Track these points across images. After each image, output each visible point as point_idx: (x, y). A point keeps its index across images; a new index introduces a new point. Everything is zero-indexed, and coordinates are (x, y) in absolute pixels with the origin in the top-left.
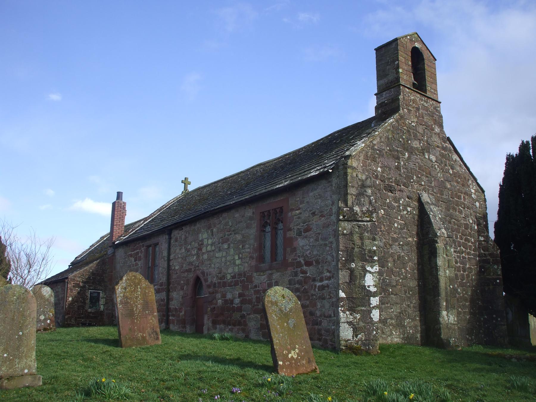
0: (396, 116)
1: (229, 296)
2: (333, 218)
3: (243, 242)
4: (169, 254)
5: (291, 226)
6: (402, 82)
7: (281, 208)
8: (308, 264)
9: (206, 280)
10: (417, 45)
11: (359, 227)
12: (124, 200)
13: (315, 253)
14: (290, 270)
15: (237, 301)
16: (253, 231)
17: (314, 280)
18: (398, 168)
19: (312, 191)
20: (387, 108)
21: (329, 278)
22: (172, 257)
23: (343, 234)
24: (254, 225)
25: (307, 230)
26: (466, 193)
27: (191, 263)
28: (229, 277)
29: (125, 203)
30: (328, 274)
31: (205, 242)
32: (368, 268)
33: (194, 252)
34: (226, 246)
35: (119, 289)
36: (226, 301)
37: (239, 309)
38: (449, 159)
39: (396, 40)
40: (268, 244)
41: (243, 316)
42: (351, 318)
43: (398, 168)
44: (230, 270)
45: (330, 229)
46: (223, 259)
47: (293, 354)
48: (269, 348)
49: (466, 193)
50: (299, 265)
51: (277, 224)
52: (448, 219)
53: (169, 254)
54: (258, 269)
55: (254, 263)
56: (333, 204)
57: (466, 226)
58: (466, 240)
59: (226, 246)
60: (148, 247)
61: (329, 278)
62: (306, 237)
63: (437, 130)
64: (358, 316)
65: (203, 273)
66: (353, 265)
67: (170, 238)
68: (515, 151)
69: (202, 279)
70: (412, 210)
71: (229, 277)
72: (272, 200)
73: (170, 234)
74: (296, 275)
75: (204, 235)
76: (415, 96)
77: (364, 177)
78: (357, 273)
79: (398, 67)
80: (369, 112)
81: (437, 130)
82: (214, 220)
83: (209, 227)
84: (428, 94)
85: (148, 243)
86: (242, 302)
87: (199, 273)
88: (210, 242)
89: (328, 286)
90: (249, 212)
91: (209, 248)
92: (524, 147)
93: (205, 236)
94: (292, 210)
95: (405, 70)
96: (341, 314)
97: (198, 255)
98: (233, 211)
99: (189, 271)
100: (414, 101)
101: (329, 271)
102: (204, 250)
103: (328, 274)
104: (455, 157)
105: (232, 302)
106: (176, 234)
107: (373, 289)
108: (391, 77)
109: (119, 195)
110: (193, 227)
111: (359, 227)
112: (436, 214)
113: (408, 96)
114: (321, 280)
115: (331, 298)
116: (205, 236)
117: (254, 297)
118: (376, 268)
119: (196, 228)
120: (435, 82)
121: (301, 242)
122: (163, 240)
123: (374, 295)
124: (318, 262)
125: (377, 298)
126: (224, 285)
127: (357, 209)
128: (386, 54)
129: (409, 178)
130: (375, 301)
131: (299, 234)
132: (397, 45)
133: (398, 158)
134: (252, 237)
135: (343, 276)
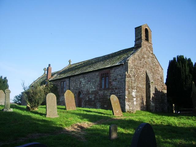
0: (141, 48)
1: (90, 97)
2: (124, 77)
3: (95, 82)
4: (69, 84)
5: (111, 78)
6: (142, 39)
7: (108, 73)
8: (116, 89)
9: (83, 93)
10: (147, 28)
11: (131, 79)
12: (51, 67)
13: (118, 86)
14: (110, 90)
15: (93, 99)
16: (98, 79)
17: (118, 93)
18: (141, 63)
19: (117, 69)
20: (138, 46)
21: (122, 93)
22: (70, 85)
23: (127, 81)
24: (99, 77)
25: (116, 79)
26: (158, 70)
27: (77, 87)
28: (90, 92)
29: (51, 68)
30: (122, 92)
31: (82, 81)
32: (133, 91)
33: (78, 84)
34: (89, 83)
35: (65, 94)
36: (89, 99)
37: (94, 101)
38: (154, 60)
39: (141, 26)
40: (103, 83)
41: (95, 103)
42: (128, 104)
43: (141, 63)
44: (91, 90)
45: (123, 80)
46: (89, 87)
47: (117, 112)
48: (112, 111)
49: (158, 70)
50: (113, 89)
51: (106, 77)
52: (153, 78)
53: (69, 84)
54: (100, 90)
55: (99, 88)
56: (124, 73)
57: (158, 79)
58: (158, 83)
59: (89, 83)
60: (61, 82)
61: (122, 93)
62: (115, 81)
63: (151, 52)
64: (130, 103)
65: (82, 91)
66: (129, 90)
67: (70, 80)
68: (172, 59)
69: (81, 92)
70: (144, 76)
71: (90, 92)
72: (104, 70)
73: (70, 78)
74: (112, 92)
75: (82, 80)
76: (146, 43)
77: (132, 66)
78: (130, 92)
79: (141, 34)
80: (132, 45)
81: (151, 52)
82: (85, 75)
83: (84, 77)
84: (149, 42)
85: (61, 81)
86: (94, 99)
87: (80, 90)
88: (84, 81)
89: (122, 95)
90: (97, 73)
91: (84, 83)
92: (174, 59)
93: (82, 79)
94: (111, 74)
95: (142, 35)
96: (126, 102)
97: (80, 85)
98: (92, 73)
99: (77, 90)
100: (145, 44)
101: (122, 91)
102: (82, 84)
103: (122, 92)
104: (156, 60)
105: (91, 99)
106: (72, 78)
107: (134, 96)
108: (139, 37)
109: (49, 65)
110: (78, 77)
111: (131, 79)
112: (150, 76)
113: (144, 42)
114: (120, 93)
115: (122, 98)
116: (82, 79)
117: (99, 98)
118: (135, 91)
119: (79, 77)
120: (151, 38)
121: (114, 83)
122: (67, 80)
123: (135, 97)
124: (119, 88)
125: (136, 99)
126: (89, 94)
127: (130, 74)
128: (138, 30)
129: (143, 66)
130: (135, 99)
131: (113, 80)
132: (141, 27)
133: (141, 60)
134: (98, 81)
135: (127, 92)
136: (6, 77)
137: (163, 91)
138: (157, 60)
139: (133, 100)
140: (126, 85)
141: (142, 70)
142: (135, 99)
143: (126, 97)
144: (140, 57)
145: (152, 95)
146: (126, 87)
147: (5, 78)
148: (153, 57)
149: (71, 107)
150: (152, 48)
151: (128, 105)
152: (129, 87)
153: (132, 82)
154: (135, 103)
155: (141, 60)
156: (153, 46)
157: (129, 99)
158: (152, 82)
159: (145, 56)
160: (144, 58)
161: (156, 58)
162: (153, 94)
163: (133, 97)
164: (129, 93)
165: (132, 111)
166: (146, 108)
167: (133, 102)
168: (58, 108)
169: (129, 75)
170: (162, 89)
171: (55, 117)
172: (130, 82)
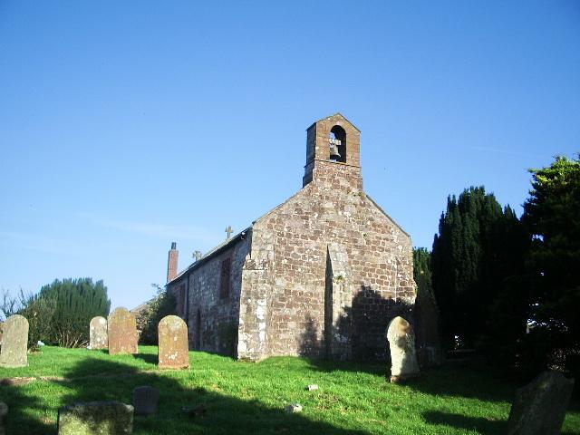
18: (307, 226)
47: (173, 357)
64: (251, 336)
107: (261, 318)
123: (262, 321)
127: (256, 260)
130: (262, 326)
133: (307, 218)
135: (243, 308)
136: (102, 282)
137: (403, 298)
138: (380, 209)
139: (256, 327)
140: (243, 289)
141: (313, 245)
142: (262, 326)
143: (241, 321)
144: (305, 208)
145: (336, 316)
146: (243, 295)
147: (100, 283)
148: (364, 205)
149: (123, 348)
150: (360, 180)
151: (245, 341)
152: (248, 293)
153: (257, 282)
154: (262, 336)
155: (307, 218)
156: (363, 174)
157: (247, 325)
158: (340, 277)
159: (328, 205)
160: (322, 211)
161: (376, 205)
162: (346, 309)
163: (259, 321)
164: (249, 310)
165: (253, 356)
166: (140, 343)
167: (258, 333)
168: (77, 347)
169: (253, 261)
170: (400, 294)
171: (17, 366)
172: (252, 282)
